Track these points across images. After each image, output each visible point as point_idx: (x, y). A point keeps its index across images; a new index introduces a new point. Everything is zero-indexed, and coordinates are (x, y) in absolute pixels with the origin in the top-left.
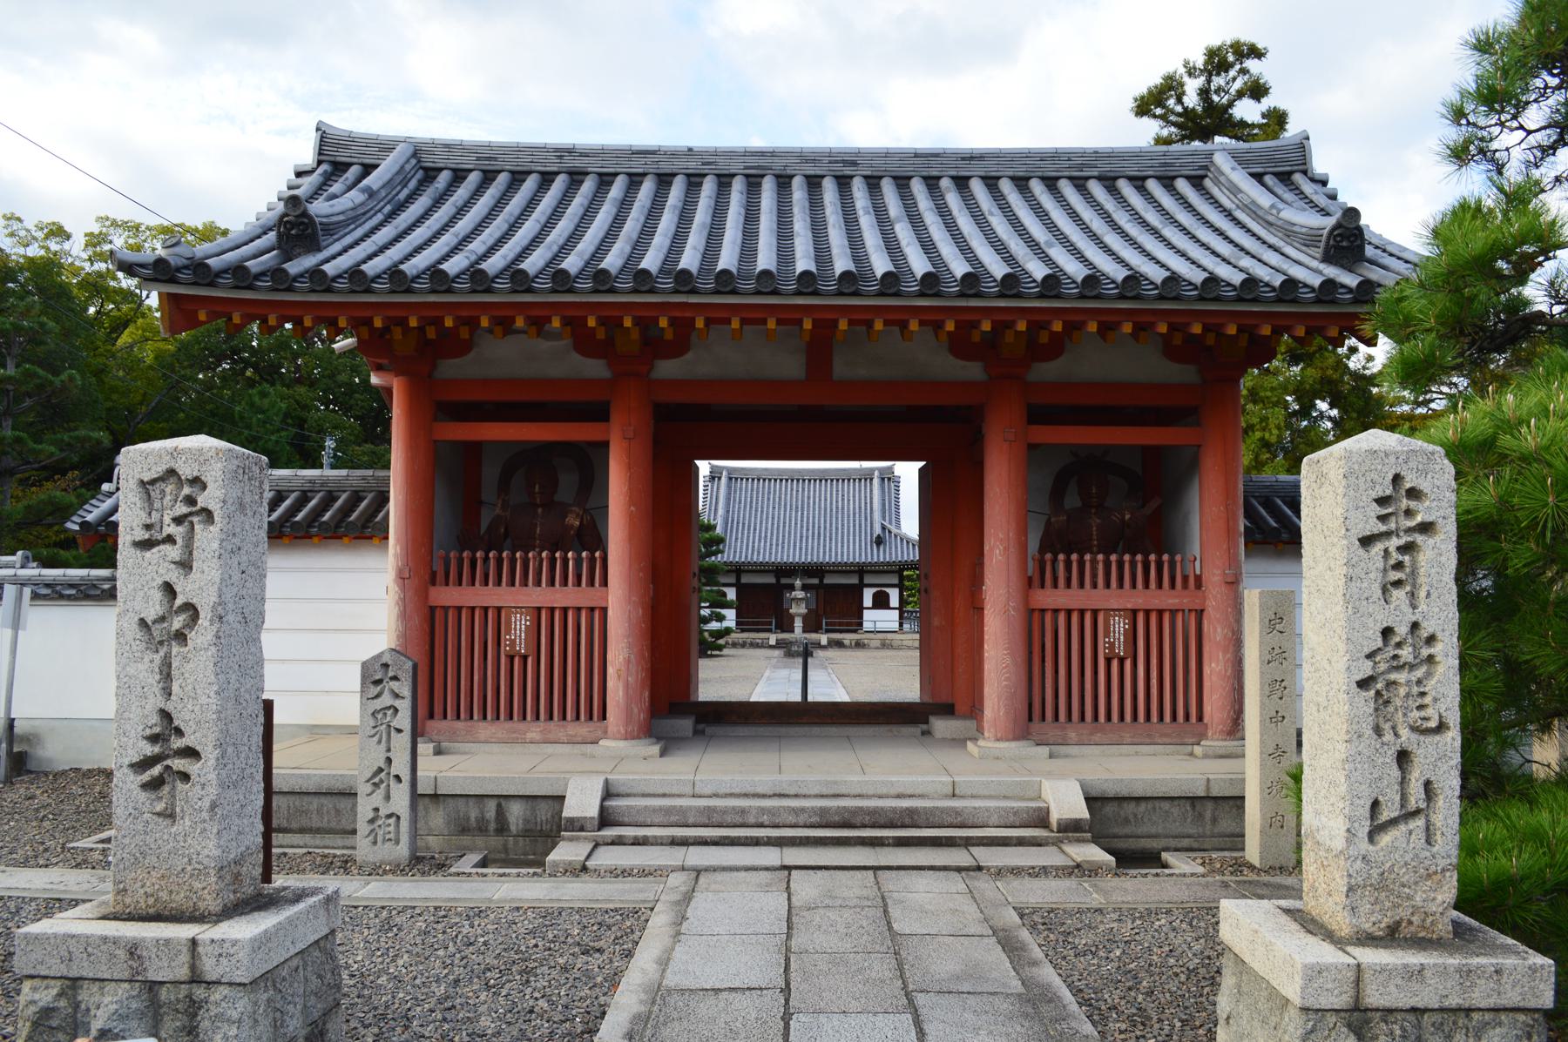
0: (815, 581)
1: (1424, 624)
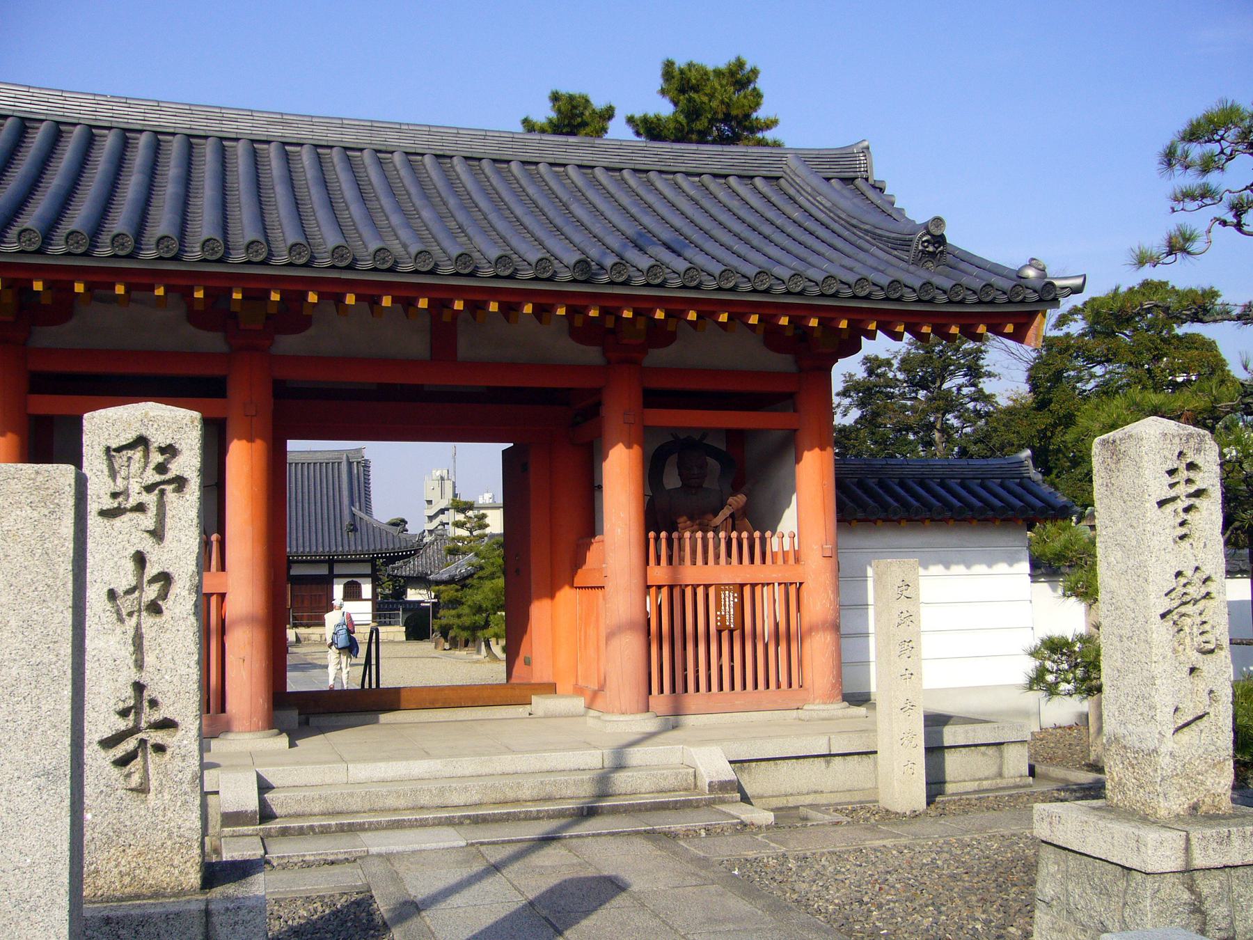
1: (1203, 568)
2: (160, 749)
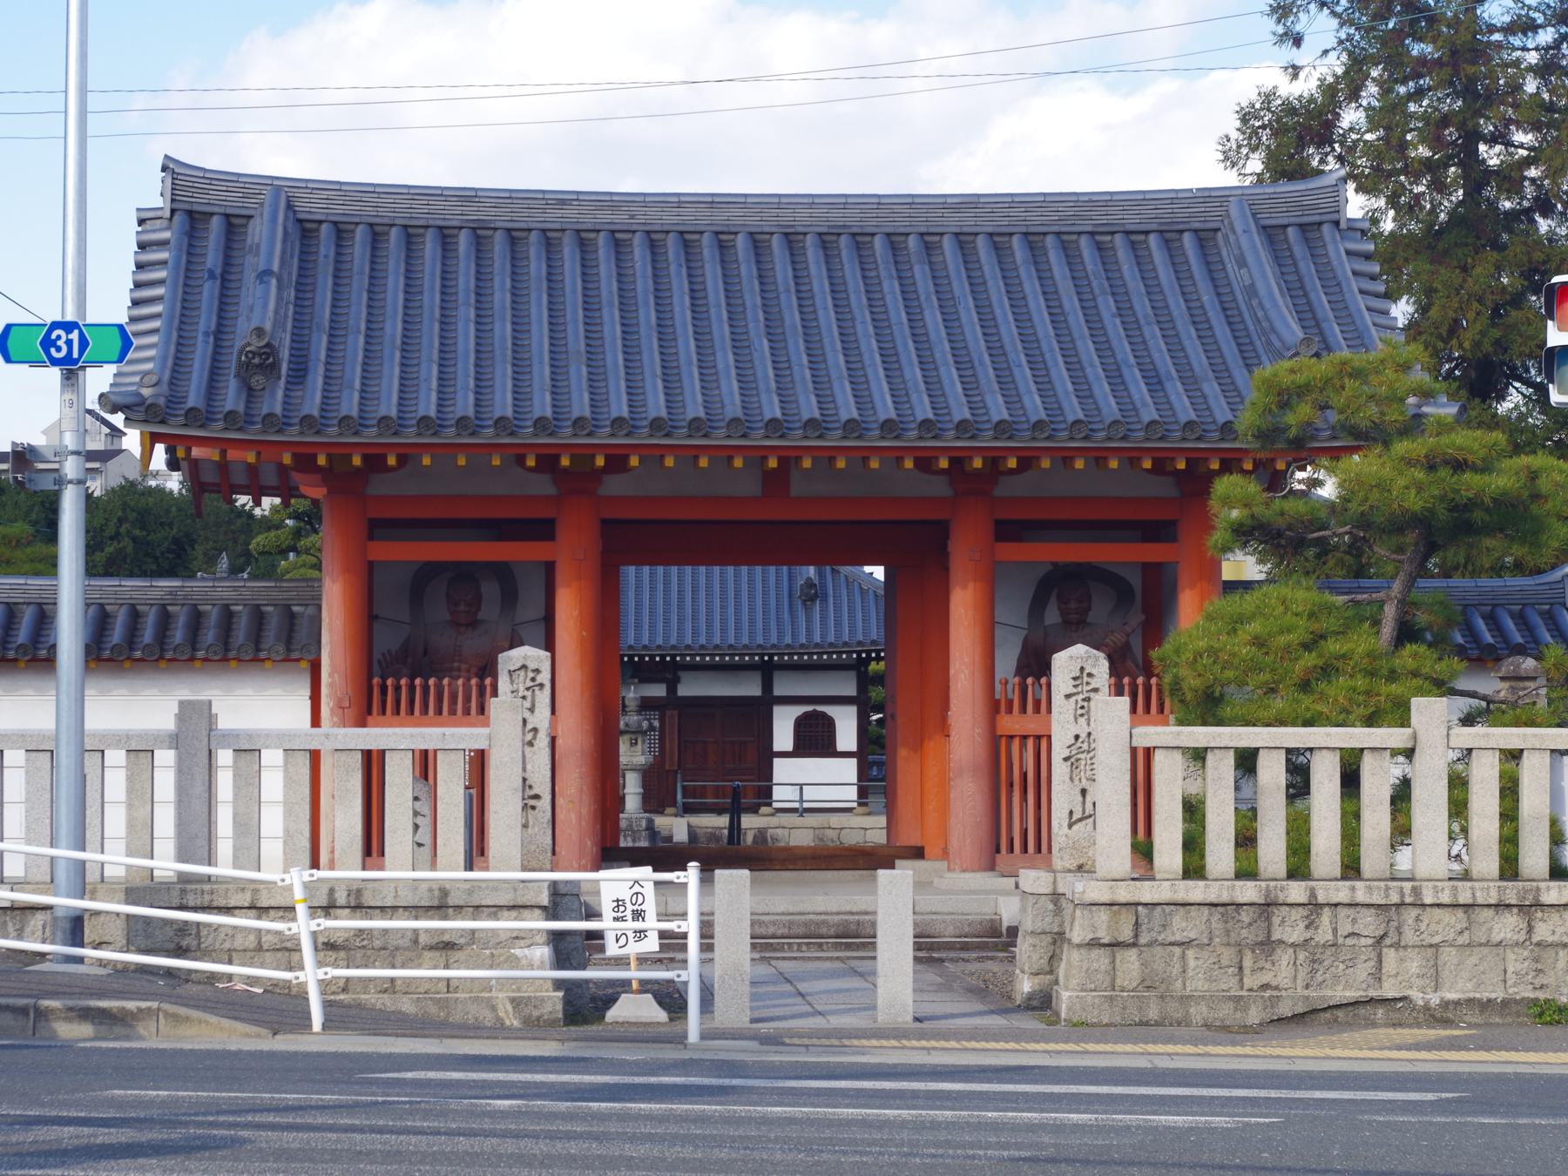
0: (658, 691)
2: (533, 808)
